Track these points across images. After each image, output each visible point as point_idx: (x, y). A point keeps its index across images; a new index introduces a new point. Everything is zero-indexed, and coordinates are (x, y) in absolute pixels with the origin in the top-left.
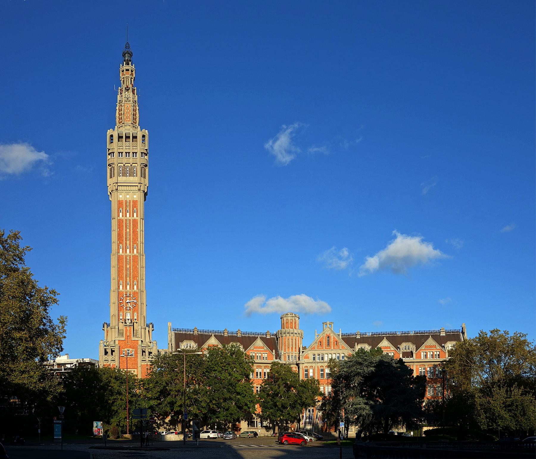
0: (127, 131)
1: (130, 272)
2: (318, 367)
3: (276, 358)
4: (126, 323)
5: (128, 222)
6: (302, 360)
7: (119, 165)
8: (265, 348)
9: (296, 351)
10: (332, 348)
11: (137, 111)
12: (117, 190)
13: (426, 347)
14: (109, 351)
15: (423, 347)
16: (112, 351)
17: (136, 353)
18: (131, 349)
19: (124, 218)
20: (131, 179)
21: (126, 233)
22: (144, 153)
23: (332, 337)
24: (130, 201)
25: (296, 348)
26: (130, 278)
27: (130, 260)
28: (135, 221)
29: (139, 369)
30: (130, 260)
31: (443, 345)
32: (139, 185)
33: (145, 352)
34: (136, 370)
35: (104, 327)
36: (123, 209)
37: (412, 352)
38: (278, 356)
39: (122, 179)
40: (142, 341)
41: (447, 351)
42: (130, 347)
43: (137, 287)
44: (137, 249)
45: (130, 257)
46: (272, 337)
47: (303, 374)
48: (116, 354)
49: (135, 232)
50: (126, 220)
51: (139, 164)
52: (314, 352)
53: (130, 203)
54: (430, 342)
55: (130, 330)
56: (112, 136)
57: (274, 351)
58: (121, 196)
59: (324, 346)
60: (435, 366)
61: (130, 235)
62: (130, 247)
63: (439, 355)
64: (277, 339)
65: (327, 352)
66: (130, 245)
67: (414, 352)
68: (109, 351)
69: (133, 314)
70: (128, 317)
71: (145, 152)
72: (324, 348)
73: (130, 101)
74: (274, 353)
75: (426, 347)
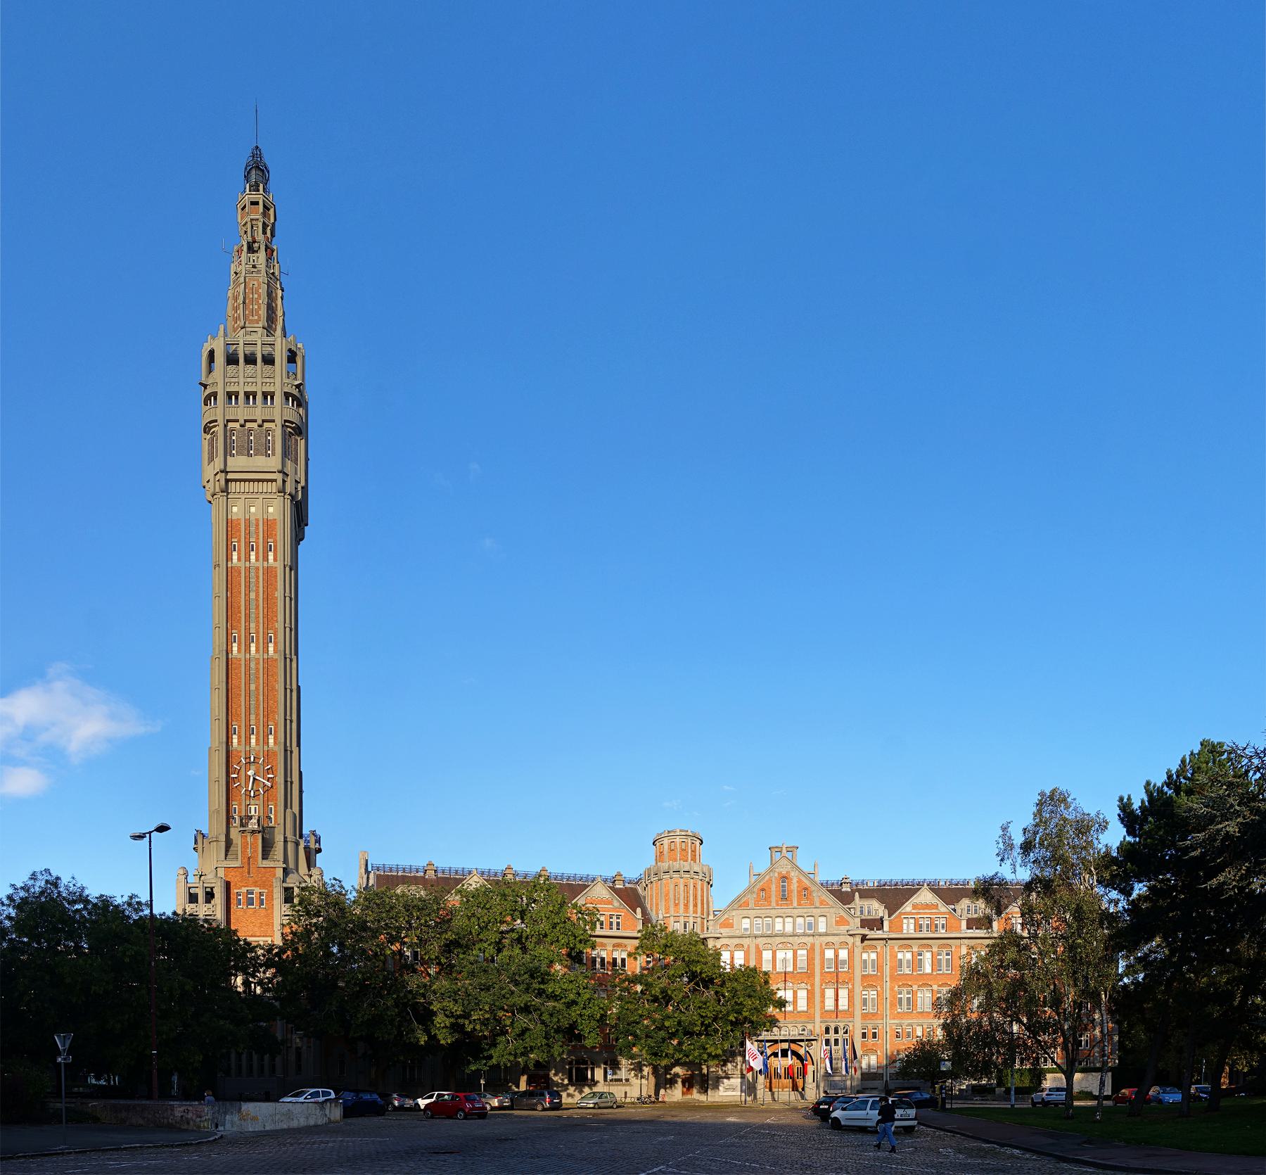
1: (258, 700)
2: (757, 946)
5: (252, 574)
8: (616, 904)
9: (695, 912)
10: (795, 904)
12: (225, 490)
15: (907, 907)
18: (257, 890)
19: (242, 564)
20: (259, 462)
21: (248, 601)
23: (795, 880)
24: (257, 520)
26: (257, 715)
27: (257, 669)
28: (269, 571)
30: (257, 669)
32: (279, 477)
35: (196, 842)
36: (239, 542)
37: (881, 920)
44: (276, 644)
45: (258, 663)
49: (268, 598)
50: (248, 570)
51: (279, 422)
53: (257, 525)
57: (639, 910)
59: (773, 899)
62: (258, 637)
65: (780, 912)
66: (257, 633)
72: (774, 904)
73: (259, 272)
75: (914, 907)
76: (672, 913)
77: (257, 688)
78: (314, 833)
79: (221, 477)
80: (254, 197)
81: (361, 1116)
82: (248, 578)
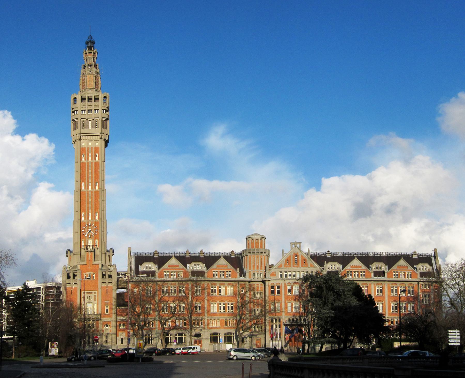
0: (89, 95)
2: (285, 284)
3: (241, 276)
4: (87, 249)
6: (268, 277)
7: (82, 119)
9: (261, 269)
11: (99, 80)
12: (80, 139)
13: (352, 267)
14: (71, 275)
16: (75, 276)
17: (97, 276)
18: (92, 273)
19: (86, 161)
20: (93, 130)
22: (106, 110)
24: (92, 148)
25: (261, 266)
26: (92, 210)
27: (92, 195)
29: (100, 290)
31: (415, 266)
32: (101, 135)
33: (105, 275)
34: (96, 291)
35: (67, 253)
36: (85, 154)
38: (242, 273)
39: (84, 130)
40: (102, 265)
41: (418, 272)
42: (91, 271)
43: (99, 217)
46: (236, 256)
47: (269, 291)
48: (78, 278)
50: (88, 163)
51: (100, 118)
52: (281, 270)
54: (402, 262)
55: (91, 256)
56: (75, 98)
57: (238, 269)
58: (83, 144)
60: (327, 318)
61: (92, 174)
63: (411, 275)
64: (242, 258)
67: (386, 271)
68: (71, 275)
69: (94, 241)
70: (90, 243)
71: (107, 109)
72: (292, 265)
74: (238, 271)
75: (352, 267)
76: (252, 269)
77: (92, 201)
78: (111, 249)
79: (79, 135)
80: (90, 51)
81: (163, 265)
82: (88, 165)
